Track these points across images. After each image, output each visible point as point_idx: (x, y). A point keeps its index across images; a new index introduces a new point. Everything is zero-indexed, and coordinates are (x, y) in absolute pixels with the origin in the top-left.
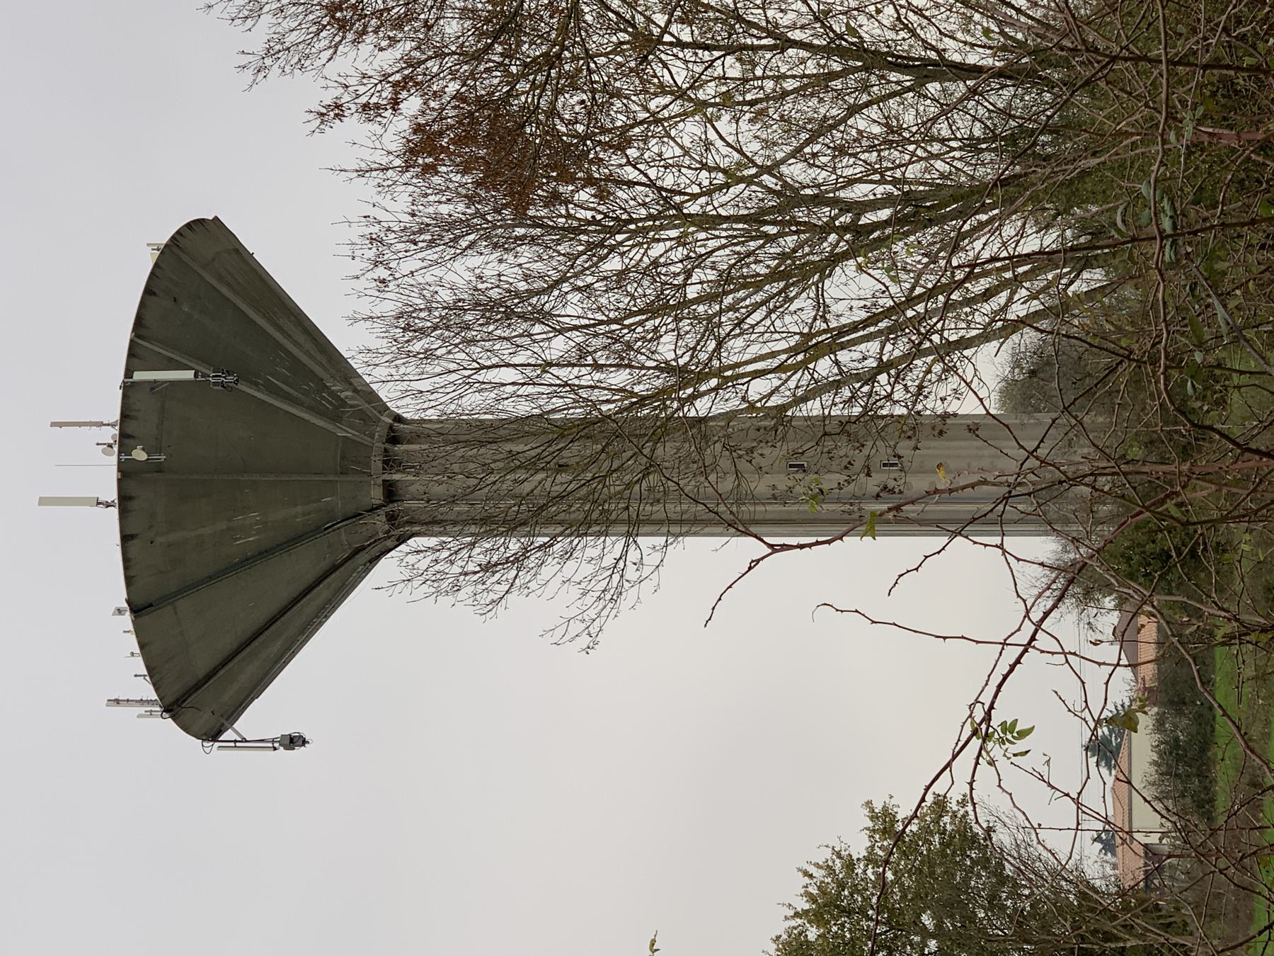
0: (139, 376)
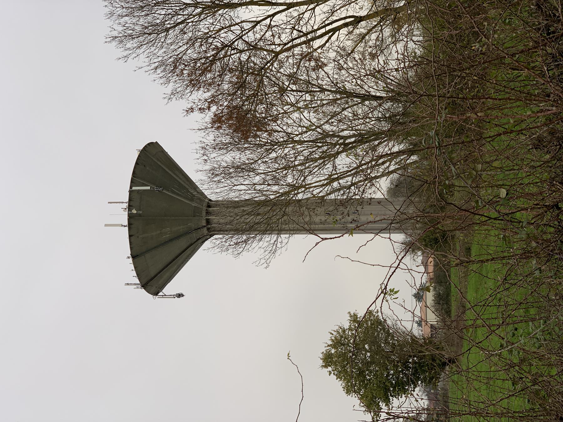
0: (134, 188)
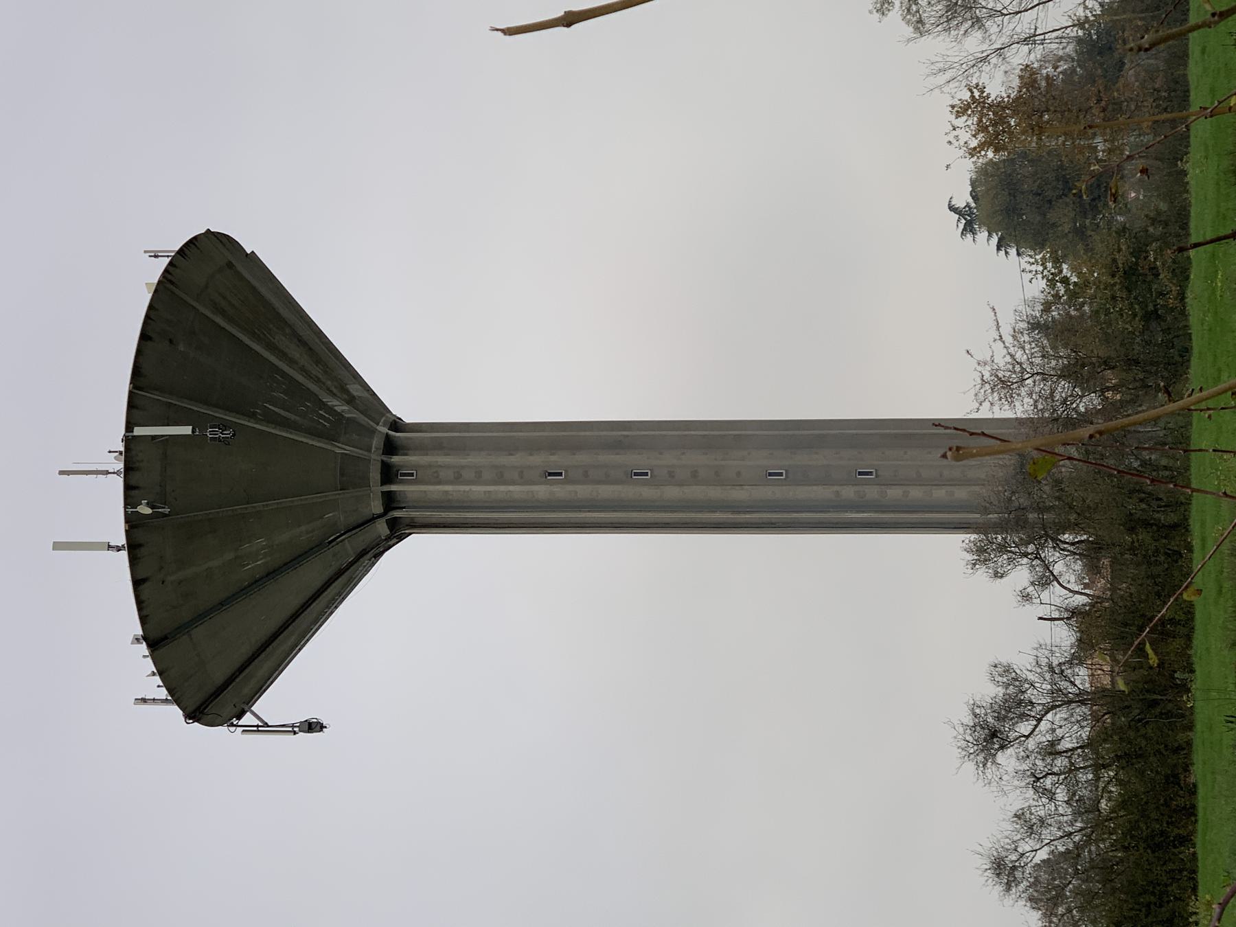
0: (138, 431)
